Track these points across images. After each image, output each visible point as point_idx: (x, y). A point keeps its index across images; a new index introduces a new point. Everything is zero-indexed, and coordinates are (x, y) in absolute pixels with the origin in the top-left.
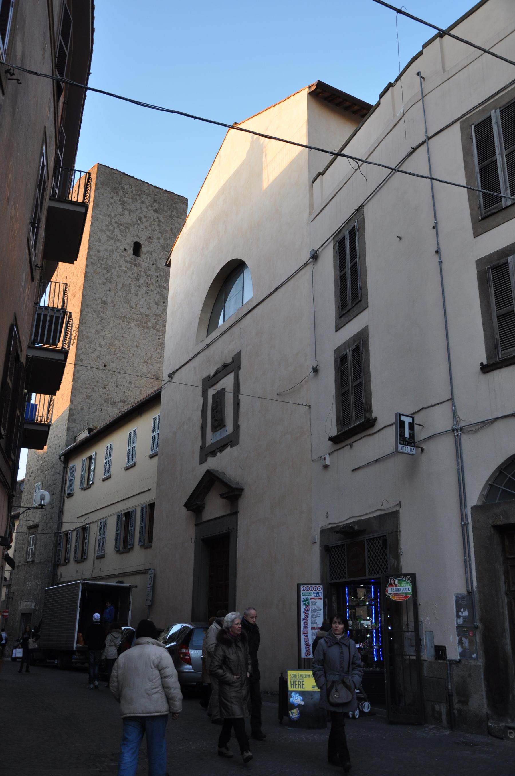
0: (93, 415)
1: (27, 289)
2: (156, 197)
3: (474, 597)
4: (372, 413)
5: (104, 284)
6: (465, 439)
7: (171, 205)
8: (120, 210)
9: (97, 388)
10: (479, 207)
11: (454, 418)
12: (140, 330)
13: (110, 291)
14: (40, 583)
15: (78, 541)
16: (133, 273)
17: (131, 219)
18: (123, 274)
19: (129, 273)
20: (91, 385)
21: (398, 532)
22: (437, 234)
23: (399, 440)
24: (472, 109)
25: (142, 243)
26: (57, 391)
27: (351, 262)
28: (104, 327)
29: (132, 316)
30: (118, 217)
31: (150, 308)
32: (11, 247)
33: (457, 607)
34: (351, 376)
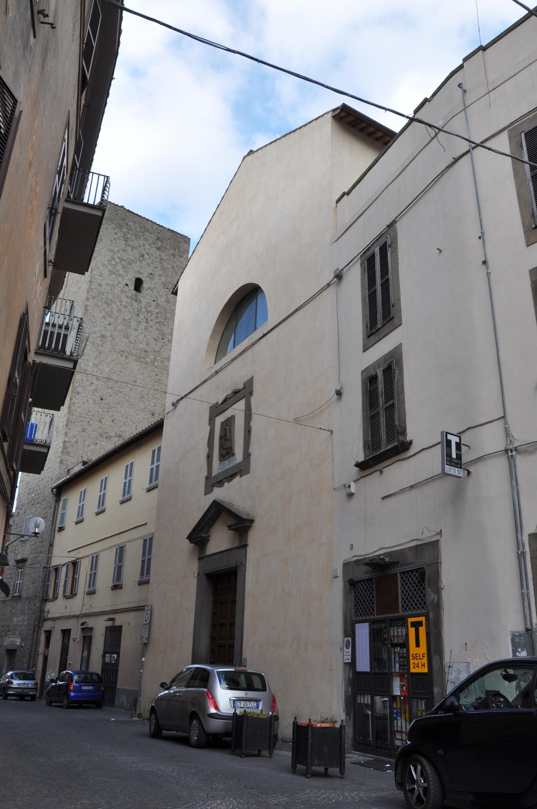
0: (88, 448)
1: (39, 283)
2: (159, 235)
3: (534, 635)
4: (407, 435)
5: (104, 317)
6: (520, 460)
7: (174, 244)
8: (123, 246)
9: (93, 421)
10: (532, 215)
11: (507, 438)
12: (138, 365)
13: (109, 325)
14: (26, 619)
15: (68, 577)
16: (133, 309)
17: (134, 256)
18: (123, 309)
19: (130, 308)
20: (86, 418)
21: (439, 563)
22: (484, 244)
23: (446, 460)
24: (522, 117)
25: (143, 279)
26: (62, 407)
27: (382, 279)
28: (102, 361)
29: (130, 351)
30: (121, 253)
31: (149, 344)
32: (28, 222)
33: (513, 646)
34: (382, 397)
